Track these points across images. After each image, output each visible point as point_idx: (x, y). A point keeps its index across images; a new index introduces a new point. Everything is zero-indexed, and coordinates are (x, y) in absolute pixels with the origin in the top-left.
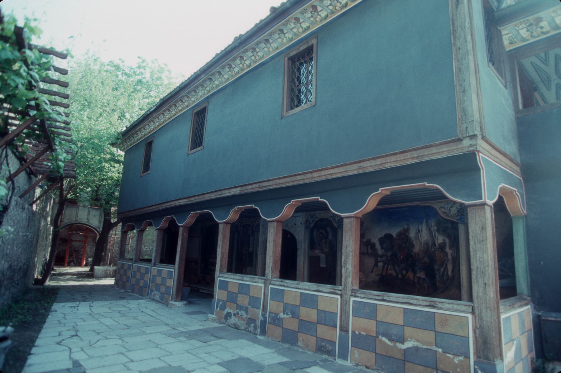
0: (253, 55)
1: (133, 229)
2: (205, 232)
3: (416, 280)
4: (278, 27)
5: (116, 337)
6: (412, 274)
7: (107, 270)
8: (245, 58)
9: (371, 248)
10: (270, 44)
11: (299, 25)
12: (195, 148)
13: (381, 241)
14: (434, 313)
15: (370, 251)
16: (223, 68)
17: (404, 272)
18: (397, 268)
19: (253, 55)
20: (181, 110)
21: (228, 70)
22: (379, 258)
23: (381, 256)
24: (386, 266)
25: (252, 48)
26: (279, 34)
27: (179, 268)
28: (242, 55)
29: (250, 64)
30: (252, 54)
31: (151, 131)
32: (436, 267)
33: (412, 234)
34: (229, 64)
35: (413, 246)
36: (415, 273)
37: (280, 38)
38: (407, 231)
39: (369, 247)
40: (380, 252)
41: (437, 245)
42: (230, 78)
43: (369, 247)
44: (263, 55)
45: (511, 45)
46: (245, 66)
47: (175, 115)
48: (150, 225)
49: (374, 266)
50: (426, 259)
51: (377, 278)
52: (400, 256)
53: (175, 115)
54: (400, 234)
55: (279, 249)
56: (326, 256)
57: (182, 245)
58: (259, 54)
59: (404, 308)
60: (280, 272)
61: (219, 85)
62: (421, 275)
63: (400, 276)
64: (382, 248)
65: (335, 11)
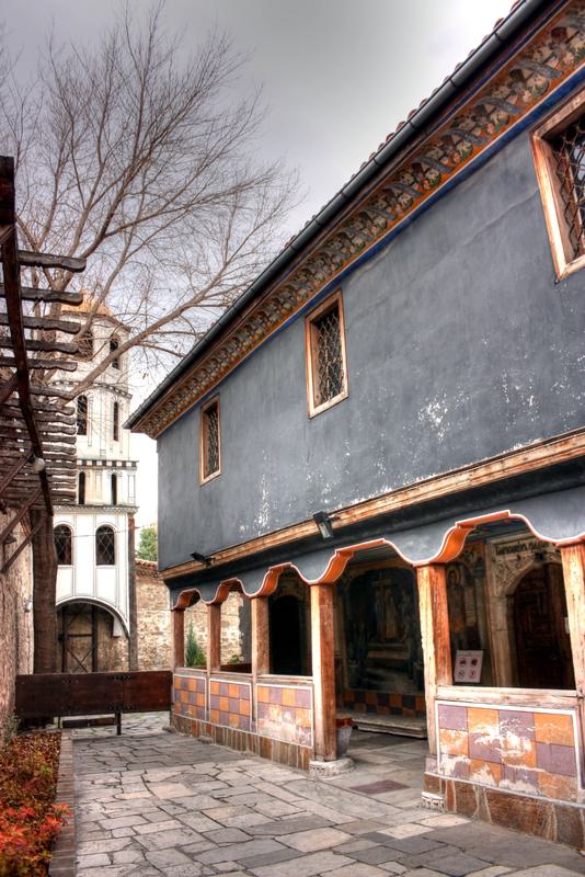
2: (373, 594)
4: (510, 65)
5: (235, 866)
7: (488, 835)
10: (488, 116)
11: (563, 46)
12: (322, 403)
19: (445, 155)
20: (277, 323)
21: (385, 204)
25: (260, 313)
27: (325, 679)
28: (416, 160)
29: (439, 177)
30: (441, 153)
31: (202, 392)
34: (385, 191)
42: (390, 222)
46: (426, 187)
47: (264, 335)
53: (264, 335)
57: (323, 628)
58: (428, 175)
61: (364, 245)
65: (452, 165)
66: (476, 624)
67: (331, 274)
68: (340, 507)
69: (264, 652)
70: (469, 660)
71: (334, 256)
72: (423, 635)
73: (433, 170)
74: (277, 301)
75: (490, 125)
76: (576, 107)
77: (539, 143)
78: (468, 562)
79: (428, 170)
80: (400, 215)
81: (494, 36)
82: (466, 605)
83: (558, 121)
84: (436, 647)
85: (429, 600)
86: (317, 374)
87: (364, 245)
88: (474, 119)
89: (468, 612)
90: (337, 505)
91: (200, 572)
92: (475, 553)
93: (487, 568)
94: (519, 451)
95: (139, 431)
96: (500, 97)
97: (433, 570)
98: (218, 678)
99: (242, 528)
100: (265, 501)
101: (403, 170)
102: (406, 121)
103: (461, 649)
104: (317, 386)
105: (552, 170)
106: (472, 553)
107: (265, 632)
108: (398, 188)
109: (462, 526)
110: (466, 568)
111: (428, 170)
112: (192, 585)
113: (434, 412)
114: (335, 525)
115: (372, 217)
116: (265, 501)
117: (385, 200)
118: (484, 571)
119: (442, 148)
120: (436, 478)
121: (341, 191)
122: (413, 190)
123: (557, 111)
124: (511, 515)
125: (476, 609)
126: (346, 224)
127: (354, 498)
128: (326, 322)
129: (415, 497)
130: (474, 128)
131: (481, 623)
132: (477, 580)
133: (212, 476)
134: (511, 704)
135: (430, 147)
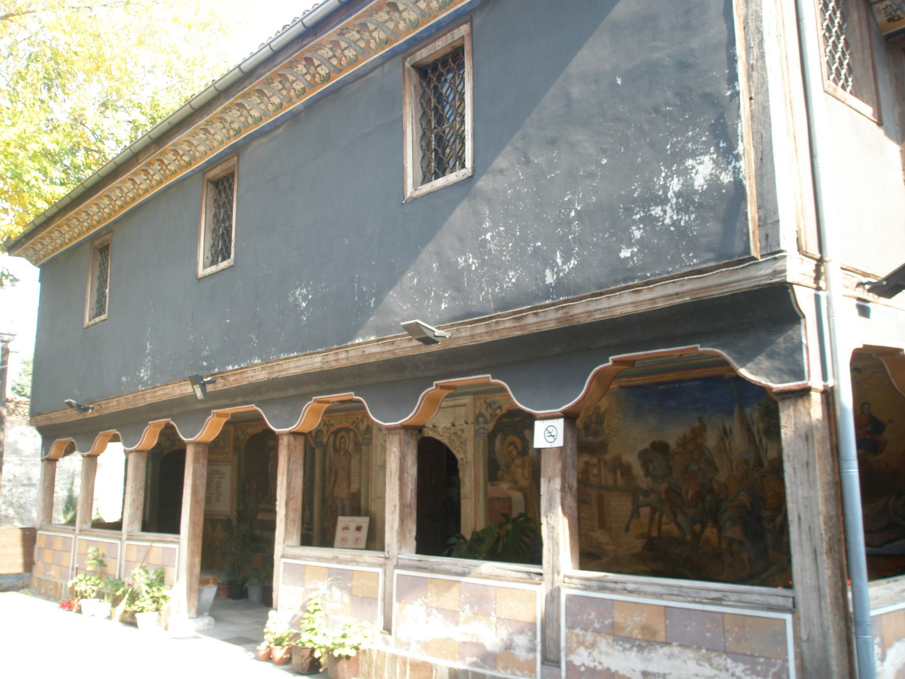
0: (334, 56)
1: (69, 450)
2: (248, 453)
3: (724, 545)
6: (715, 530)
8: (317, 62)
9: (622, 474)
13: (644, 456)
14: (723, 613)
15: (620, 481)
16: (269, 81)
17: (697, 527)
18: (680, 518)
19: (334, 56)
20: (174, 173)
21: (280, 86)
22: (641, 498)
23: (646, 494)
24: (657, 516)
25: (158, 160)
26: (388, 13)
27: (192, 537)
29: (329, 74)
32: (766, 514)
33: (711, 440)
34: (280, 75)
35: (716, 470)
36: (720, 530)
37: (391, 19)
38: (698, 434)
39: (619, 472)
40: (644, 482)
41: (766, 464)
42: (285, 104)
43: (619, 472)
44: (356, 56)
45: (892, 24)
46: (317, 79)
47: (161, 182)
48: (115, 439)
49: (632, 517)
50: (744, 498)
51: (639, 543)
52: (687, 494)
53: (161, 182)
54: (683, 442)
55: (716, 293)
56: (525, 497)
58: (319, 69)
59: (665, 607)
60: (418, 538)
61: (261, 119)
62: (733, 532)
63: (689, 537)
64: (648, 474)
66: (359, 490)
67: (229, 138)
68: (217, 370)
69: (137, 508)
70: (353, 526)
71: (232, 122)
72: (278, 498)
73: (323, 67)
74: (176, 152)
75: (372, 41)
76: (438, 48)
77: (409, 71)
78: (358, 428)
79: (320, 65)
80: (295, 100)
81: (212, 88)
82: (352, 471)
83: (424, 56)
84: (287, 510)
85: (286, 466)
86: (209, 235)
87: (261, 119)
88: (358, 32)
89: (353, 478)
90: (214, 368)
91: (409, 358)
92: (365, 420)
93: (374, 437)
94: (359, 344)
95: (19, 255)
96: (380, 20)
97: (292, 439)
98: (86, 535)
99: (124, 379)
100: (148, 354)
101: (296, 61)
102: (266, 43)
103: (344, 514)
104: (208, 246)
105: (416, 97)
106: (362, 420)
107: (830, 495)
108: (292, 75)
109: (443, 387)
110: (355, 435)
111: (320, 65)
112: (357, 390)
113: (301, 296)
114: (210, 388)
115: (268, 95)
116: (148, 354)
117: (281, 82)
118: (371, 439)
119: (331, 49)
120: (296, 357)
121: (239, 66)
122: (282, 94)
123: (424, 47)
124: (701, 349)
125: (360, 475)
126: (244, 96)
127: (228, 365)
128: (223, 183)
129: (280, 372)
130: (387, 21)
131: (363, 490)
132: (364, 448)
133: (97, 319)
134: (339, 563)
135: (320, 46)
